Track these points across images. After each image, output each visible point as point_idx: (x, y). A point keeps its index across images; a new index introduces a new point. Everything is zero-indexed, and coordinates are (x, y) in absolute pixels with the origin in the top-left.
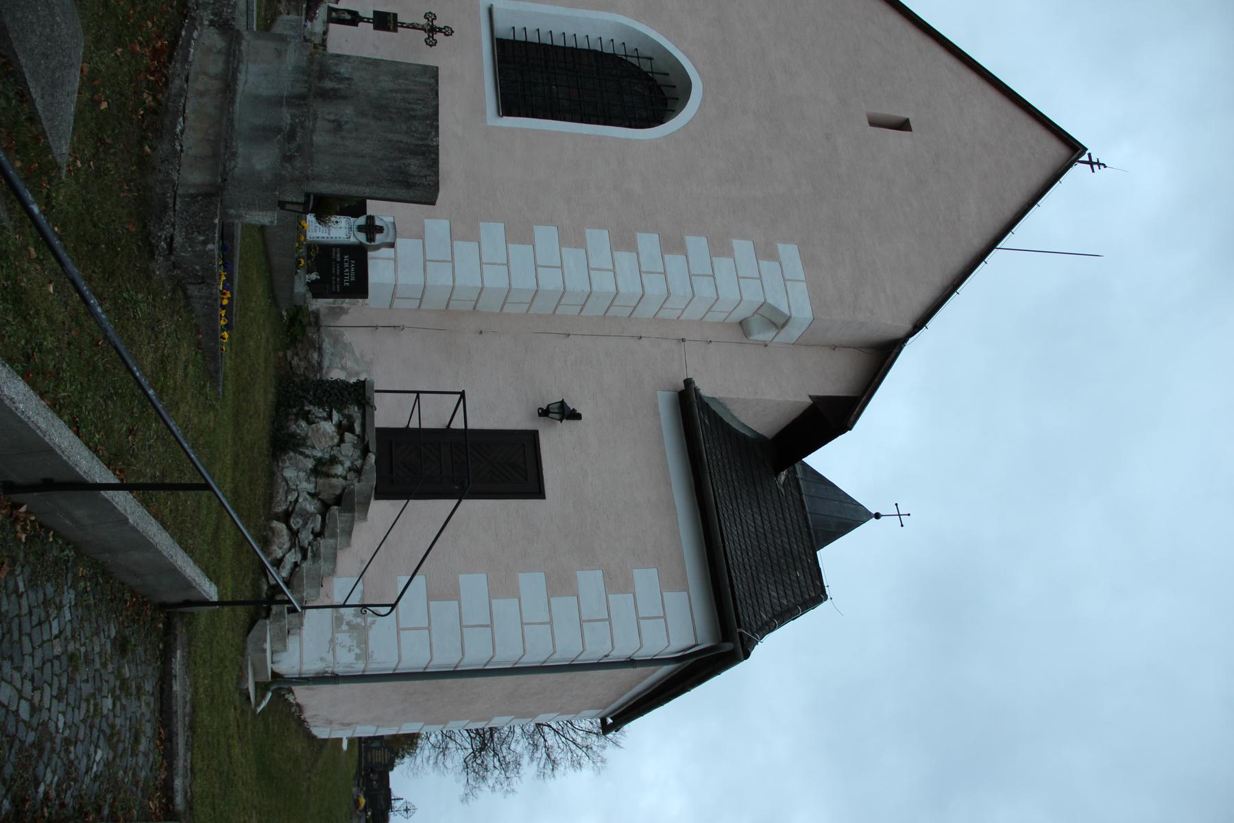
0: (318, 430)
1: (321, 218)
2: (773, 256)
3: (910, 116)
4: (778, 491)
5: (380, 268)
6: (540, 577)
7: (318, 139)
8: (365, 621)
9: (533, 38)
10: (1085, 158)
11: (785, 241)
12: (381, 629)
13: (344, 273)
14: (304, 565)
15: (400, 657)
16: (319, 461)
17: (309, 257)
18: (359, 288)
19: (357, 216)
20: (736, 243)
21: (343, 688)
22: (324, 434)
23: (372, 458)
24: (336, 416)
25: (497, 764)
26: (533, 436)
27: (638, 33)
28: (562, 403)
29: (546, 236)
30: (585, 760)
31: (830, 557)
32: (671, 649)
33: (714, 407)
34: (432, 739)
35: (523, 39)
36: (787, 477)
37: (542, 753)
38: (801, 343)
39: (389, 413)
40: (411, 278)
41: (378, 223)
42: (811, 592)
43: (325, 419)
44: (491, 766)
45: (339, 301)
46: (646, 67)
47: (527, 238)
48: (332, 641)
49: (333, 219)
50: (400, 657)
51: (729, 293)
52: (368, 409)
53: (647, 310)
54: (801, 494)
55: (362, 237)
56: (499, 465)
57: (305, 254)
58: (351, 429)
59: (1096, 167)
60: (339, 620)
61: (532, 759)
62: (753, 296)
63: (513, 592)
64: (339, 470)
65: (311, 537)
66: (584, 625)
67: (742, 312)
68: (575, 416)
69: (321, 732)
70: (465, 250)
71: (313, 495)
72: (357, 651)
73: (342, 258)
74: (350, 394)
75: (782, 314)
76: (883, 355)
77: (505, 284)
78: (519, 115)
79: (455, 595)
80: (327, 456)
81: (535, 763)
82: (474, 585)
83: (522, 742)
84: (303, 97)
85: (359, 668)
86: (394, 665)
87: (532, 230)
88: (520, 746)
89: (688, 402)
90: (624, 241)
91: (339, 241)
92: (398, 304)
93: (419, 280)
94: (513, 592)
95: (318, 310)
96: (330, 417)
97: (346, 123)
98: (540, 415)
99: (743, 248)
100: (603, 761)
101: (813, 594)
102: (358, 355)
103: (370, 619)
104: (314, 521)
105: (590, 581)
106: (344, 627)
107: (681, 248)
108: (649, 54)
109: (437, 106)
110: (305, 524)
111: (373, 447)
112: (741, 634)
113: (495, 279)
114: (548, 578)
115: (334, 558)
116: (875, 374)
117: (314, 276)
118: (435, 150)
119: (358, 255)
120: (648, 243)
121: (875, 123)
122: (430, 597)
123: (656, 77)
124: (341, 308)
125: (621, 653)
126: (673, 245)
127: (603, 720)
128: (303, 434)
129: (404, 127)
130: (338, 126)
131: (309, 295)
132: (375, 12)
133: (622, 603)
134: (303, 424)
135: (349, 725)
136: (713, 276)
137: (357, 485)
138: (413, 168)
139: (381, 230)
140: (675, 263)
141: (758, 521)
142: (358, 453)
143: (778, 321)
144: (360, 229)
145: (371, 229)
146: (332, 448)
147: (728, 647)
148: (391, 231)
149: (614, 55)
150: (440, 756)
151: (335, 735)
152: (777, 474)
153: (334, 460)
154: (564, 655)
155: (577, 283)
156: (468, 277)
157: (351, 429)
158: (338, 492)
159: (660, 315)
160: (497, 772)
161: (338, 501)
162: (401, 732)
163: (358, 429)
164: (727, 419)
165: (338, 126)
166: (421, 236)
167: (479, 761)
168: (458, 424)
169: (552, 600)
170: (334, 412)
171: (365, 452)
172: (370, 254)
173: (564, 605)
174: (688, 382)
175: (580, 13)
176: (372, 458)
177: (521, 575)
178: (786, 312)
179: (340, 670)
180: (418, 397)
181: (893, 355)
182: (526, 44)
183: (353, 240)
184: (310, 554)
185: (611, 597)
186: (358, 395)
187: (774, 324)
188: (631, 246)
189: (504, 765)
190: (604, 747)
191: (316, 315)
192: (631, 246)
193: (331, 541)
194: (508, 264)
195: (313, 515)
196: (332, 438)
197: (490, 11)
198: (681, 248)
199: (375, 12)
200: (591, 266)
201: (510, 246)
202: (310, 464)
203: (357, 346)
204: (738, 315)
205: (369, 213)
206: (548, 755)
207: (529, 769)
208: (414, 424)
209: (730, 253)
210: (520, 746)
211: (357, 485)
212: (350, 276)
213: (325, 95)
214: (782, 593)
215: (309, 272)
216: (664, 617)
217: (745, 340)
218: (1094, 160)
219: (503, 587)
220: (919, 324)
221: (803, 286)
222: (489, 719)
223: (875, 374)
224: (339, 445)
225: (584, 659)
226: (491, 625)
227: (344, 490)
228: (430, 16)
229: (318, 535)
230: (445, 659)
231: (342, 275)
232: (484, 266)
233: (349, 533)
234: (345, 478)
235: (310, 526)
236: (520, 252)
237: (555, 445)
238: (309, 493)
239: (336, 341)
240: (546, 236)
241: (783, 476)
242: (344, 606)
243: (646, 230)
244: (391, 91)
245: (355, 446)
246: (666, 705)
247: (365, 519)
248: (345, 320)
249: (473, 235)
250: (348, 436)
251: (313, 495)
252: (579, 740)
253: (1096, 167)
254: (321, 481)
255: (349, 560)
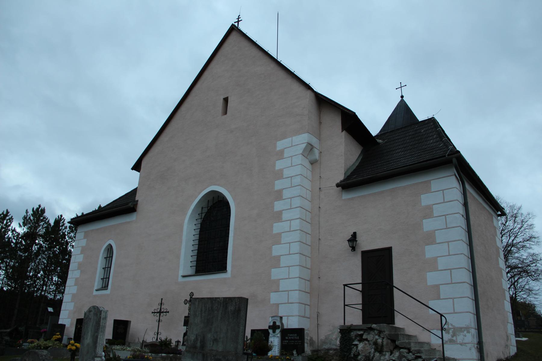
0: (362, 351)
1: (269, 349)
2: (282, 152)
3: (222, 98)
4: (386, 142)
5: (291, 323)
6: (427, 248)
7: (220, 350)
8: (451, 329)
9: (195, 258)
10: (236, 24)
11: (275, 147)
12: (453, 321)
13: (293, 338)
14: (424, 357)
15: (467, 312)
16: (376, 350)
17: (286, 354)
18: (300, 332)
19: (269, 333)
20: (277, 168)
21: (484, 339)
22: (364, 347)
23: (374, 326)
24: (356, 342)
25: (534, 265)
26: (364, 253)
27: (192, 214)
28: (348, 241)
29: (277, 250)
30: (529, 223)
31: (421, 117)
32: (458, 186)
33: (349, 173)
34: (525, 296)
35: (195, 262)
36: (380, 139)
37: (527, 244)
38: (319, 137)
39: (355, 318)
40: (295, 309)
41: (271, 324)
42: (432, 123)
43: (357, 347)
44: (535, 268)
45: (306, 341)
46: (205, 210)
47: (277, 259)
48: (461, 344)
49: (269, 344)
50: (467, 312)
51: (298, 170)
52: (352, 328)
53: (307, 205)
54: (387, 133)
55: (278, 331)
56: (377, 267)
57: (285, 356)
58: (361, 335)
59: (240, 19)
60: (451, 341)
61: (530, 248)
62: (299, 159)
63: (435, 260)
64: (380, 341)
65: (411, 354)
66: (448, 227)
67: (307, 164)
68: (354, 235)
69: (513, 350)
70: (283, 285)
71: (392, 353)
72: (465, 332)
73: (287, 340)
74: (346, 336)
75: (306, 146)
76: (322, 102)
77: (298, 268)
78: (226, 263)
79: (437, 287)
80: (374, 346)
81: (532, 246)
82: (432, 278)
83: (523, 253)
84: (203, 355)
85: (474, 332)
86: (472, 315)
87: (274, 256)
88: (524, 254)
89: (346, 185)
90: (278, 217)
91: (280, 341)
92: (308, 315)
93: (296, 305)
94: (435, 260)
95: (311, 351)
96: (356, 345)
97: (214, 337)
98: (354, 250)
99: (279, 165)
100: (529, 214)
101: (432, 124)
102: (331, 333)
103: (450, 327)
104: (403, 352)
105: (428, 225)
106: (454, 338)
107: (280, 192)
108: (200, 209)
109: (208, 298)
110: (405, 357)
111: (369, 325)
112: (448, 155)
113: (296, 272)
114: (428, 244)
115: (422, 344)
116: (331, 104)
117: (295, 352)
118: (225, 299)
119: (286, 333)
120: (278, 206)
121: (225, 112)
122: (439, 298)
123: (210, 205)
124: (310, 340)
125: (460, 209)
126: (279, 195)
127: (499, 215)
128: (364, 358)
129: (216, 312)
130: (216, 340)
131: (304, 354)
132: (184, 326)
133: (437, 210)
134: (360, 357)
135: (507, 336)
136: (291, 177)
137: (386, 333)
138: (232, 308)
139: (274, 323)
140: (286, 194)
141: (408, 150)
142: (372, 332)
143: (310, 148)
144: (274, 332)
145: (274, 327)
146: (370, 344)
147: (454, 160)
148: (275, 318)
149: (201, 224)
150: (534, 292)
151: (514, 343)
152: (378, 144)
153: (375, 343)
154: (463, 236)
155: (296, 236)
156: (295, 284)
157: (361, 335)
158: (389, 341)
159: (310, 199)
160: (538, 265)
161: (393, 341)
162: (511, 311)
163: (361, 332)
164: (354, 167)
165: (216, 340)
166: (277, 305)
167: (533, 274)
168: (360, 287)
169: (437, 242)
170: (354, 343)
171: (371, 329)
172: (285, 327)
173: (440, 237)
174: (338, 185)
175: (184, 238)
176: (374, 326)
177: (427, 256)
178: (305, 145)
179: (476, 341)
180: (347, 305)
181: (322, 97)
182: (198, 261)
183: (279, 335)
184: (418, 355)
185: (435, 215)
186: (346, 332)
187: (311, 150)
188: (280, 213)
189: (534, 261)
190: (522, 214)
191: (313, 351)
192: (280, 213)
193: (412, 344)
194: (289, 267)
195: (400, 353)
196: (366, 344)
197: (184, 276)
198: (280, 192)
199: (184, 326)
200: (289, 230)
201: (281, 266)
202: (377, 354)
203: (325, 332)
204: (308, 165)
205: (268, 328)
206: (528, 240)
207: (536, 249)
208: (360, 307)
209: (281, 171)
210: (524, 254)
211: (386, 333)
212: (295, 336)
213: (203, 346)
214: (431, 138)
215: (293, 354)
216: (443, 190)
217: (319, 162)
218: (237, 20)
219: (432, 264)
220: (308, 87)
221: (294, 138)
222: (501, 269)
223: (331, 104)
224: (368, 341)
225: (464, 226)
226: (450, 269)
227: (389, 339)
228: (186, 302)
229: (409, 351)
230: (468, 291)
231: (295, 340)
232: (290, 277)
233: (409, 337)
234: (383, 338)
235: (405, 354)
236: (284, 261)
237: (368, 243)
238: (391, 355)
239: (324, 342)
240: (277, 250)
241: (379, 141)
242: (442, 338)
243: (273, 207)
244: (201, 317)
245: (369, 334)
246: (487, 187)
247: (403, 329)
248: (315, 338)
249: (277, 282)
250: (364, 337)
251: (392, 353)
252: (519, 226)
253: (240, 19)
254: (385, 349)
255: (423, 337)
